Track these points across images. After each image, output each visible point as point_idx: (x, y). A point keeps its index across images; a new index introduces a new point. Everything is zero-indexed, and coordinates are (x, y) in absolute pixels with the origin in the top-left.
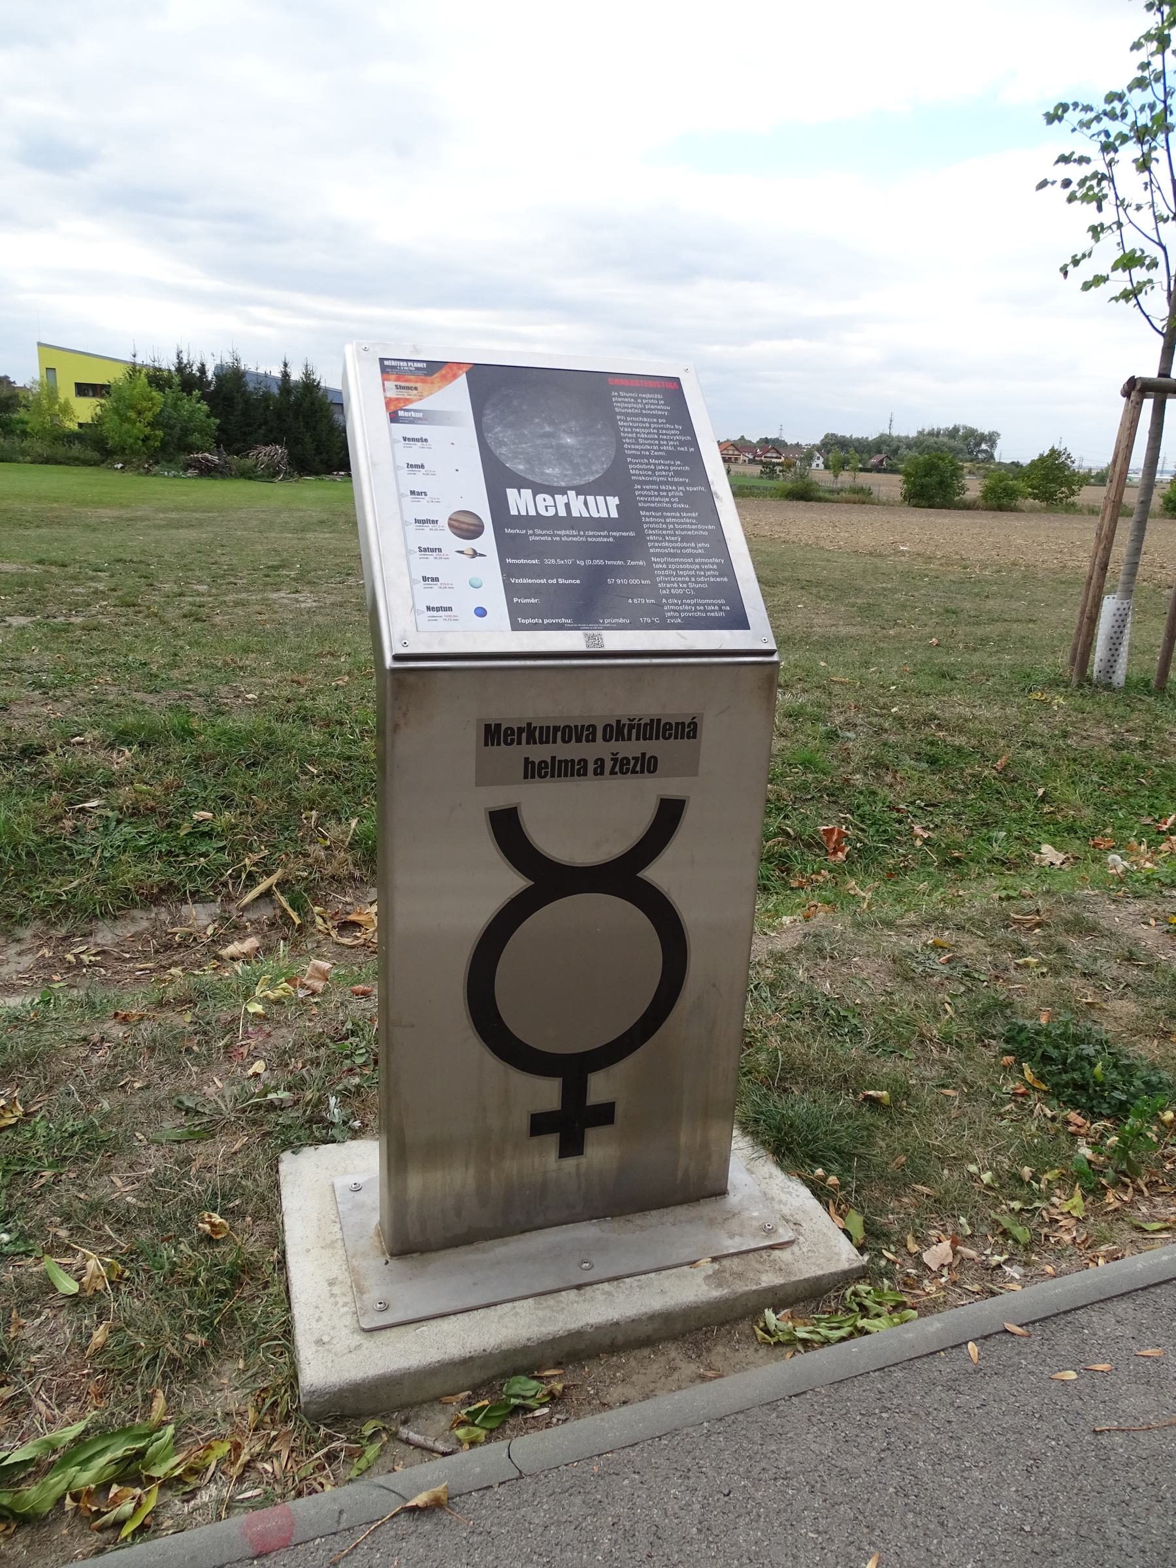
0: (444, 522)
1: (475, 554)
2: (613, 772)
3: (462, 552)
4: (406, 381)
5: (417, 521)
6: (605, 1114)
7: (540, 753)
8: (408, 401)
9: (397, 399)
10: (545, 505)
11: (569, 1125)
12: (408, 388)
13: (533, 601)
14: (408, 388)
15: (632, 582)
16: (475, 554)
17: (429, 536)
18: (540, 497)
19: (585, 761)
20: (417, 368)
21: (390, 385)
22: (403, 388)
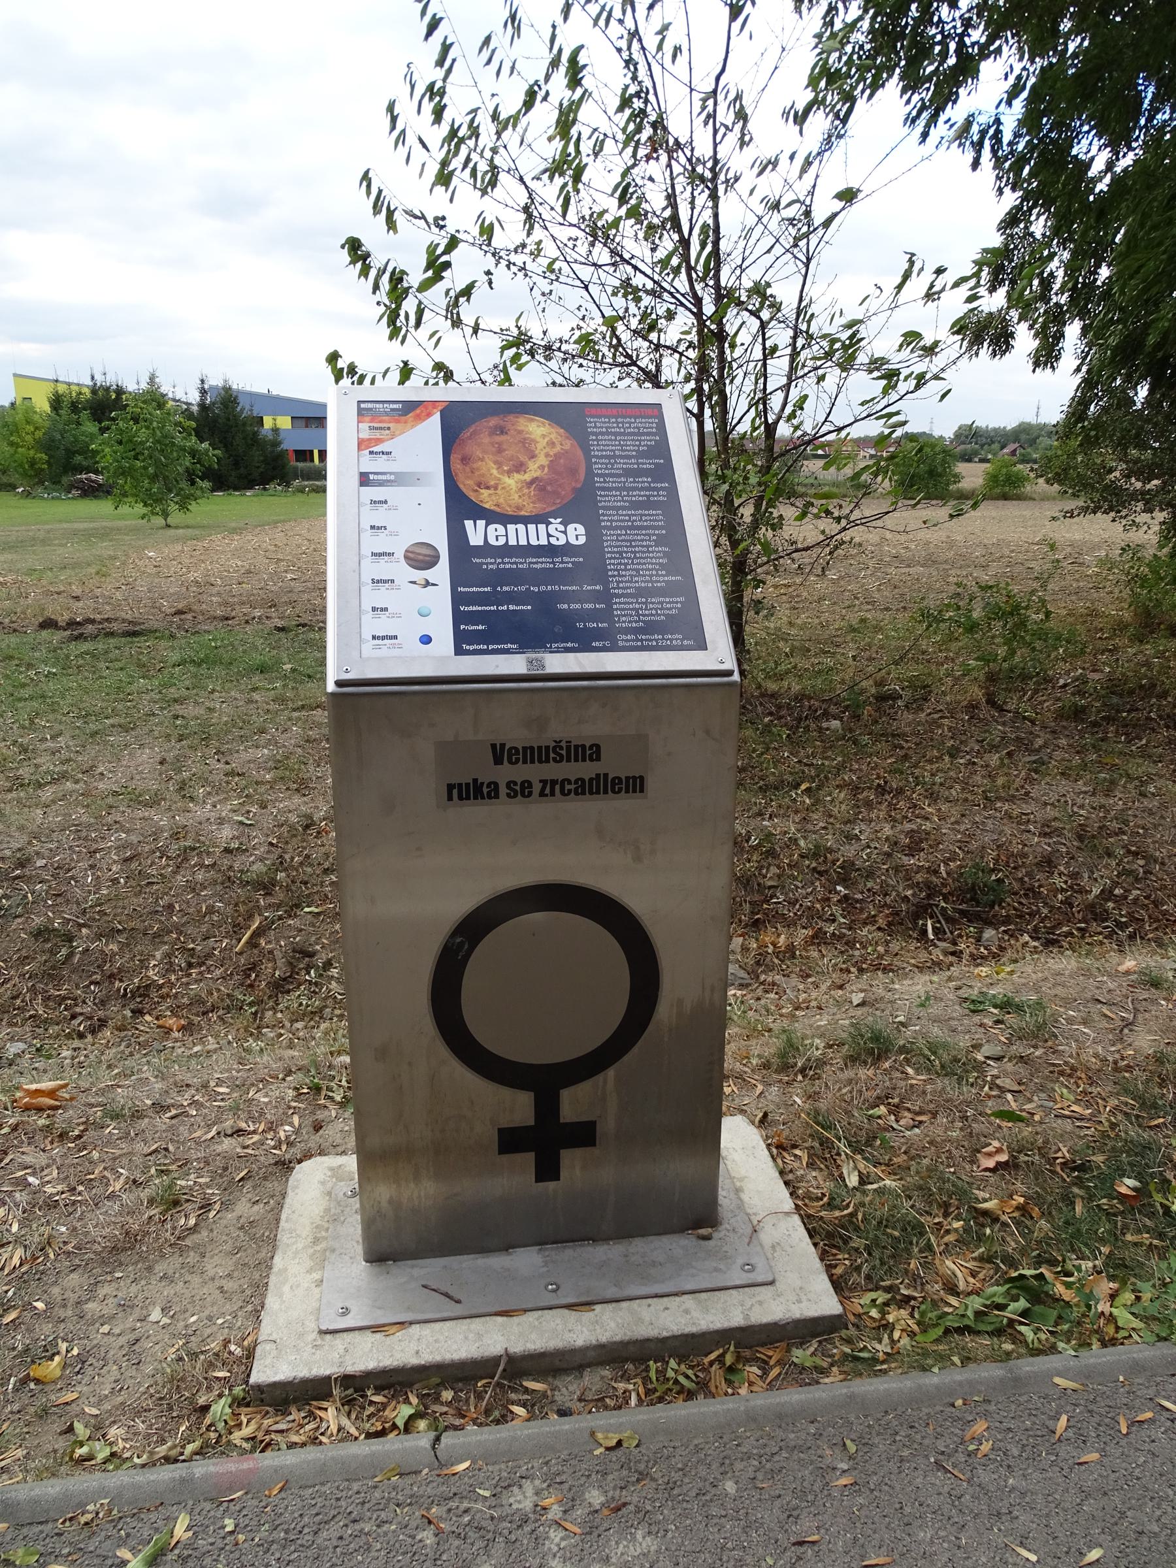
0: (400, 554)
1: (427, 584)
2: (542, 794)
3: (414, 583)
4: (380, 422)
5: (373, 554)
6: (584, 1135)
7: (585, 770)
8: (379, 441)
9: (370, 440)
10: (497, 535)
11: (544, 1142)
12: (381, 428)
13: (480, 627)
14: (381, 428)
15: (591, 606)
16: (427, 584)
17: (383, 569)
18: (492, 527)
19: (496, 784)
20: (392, 410)
21: (364, 426)
22: (377, 429)
